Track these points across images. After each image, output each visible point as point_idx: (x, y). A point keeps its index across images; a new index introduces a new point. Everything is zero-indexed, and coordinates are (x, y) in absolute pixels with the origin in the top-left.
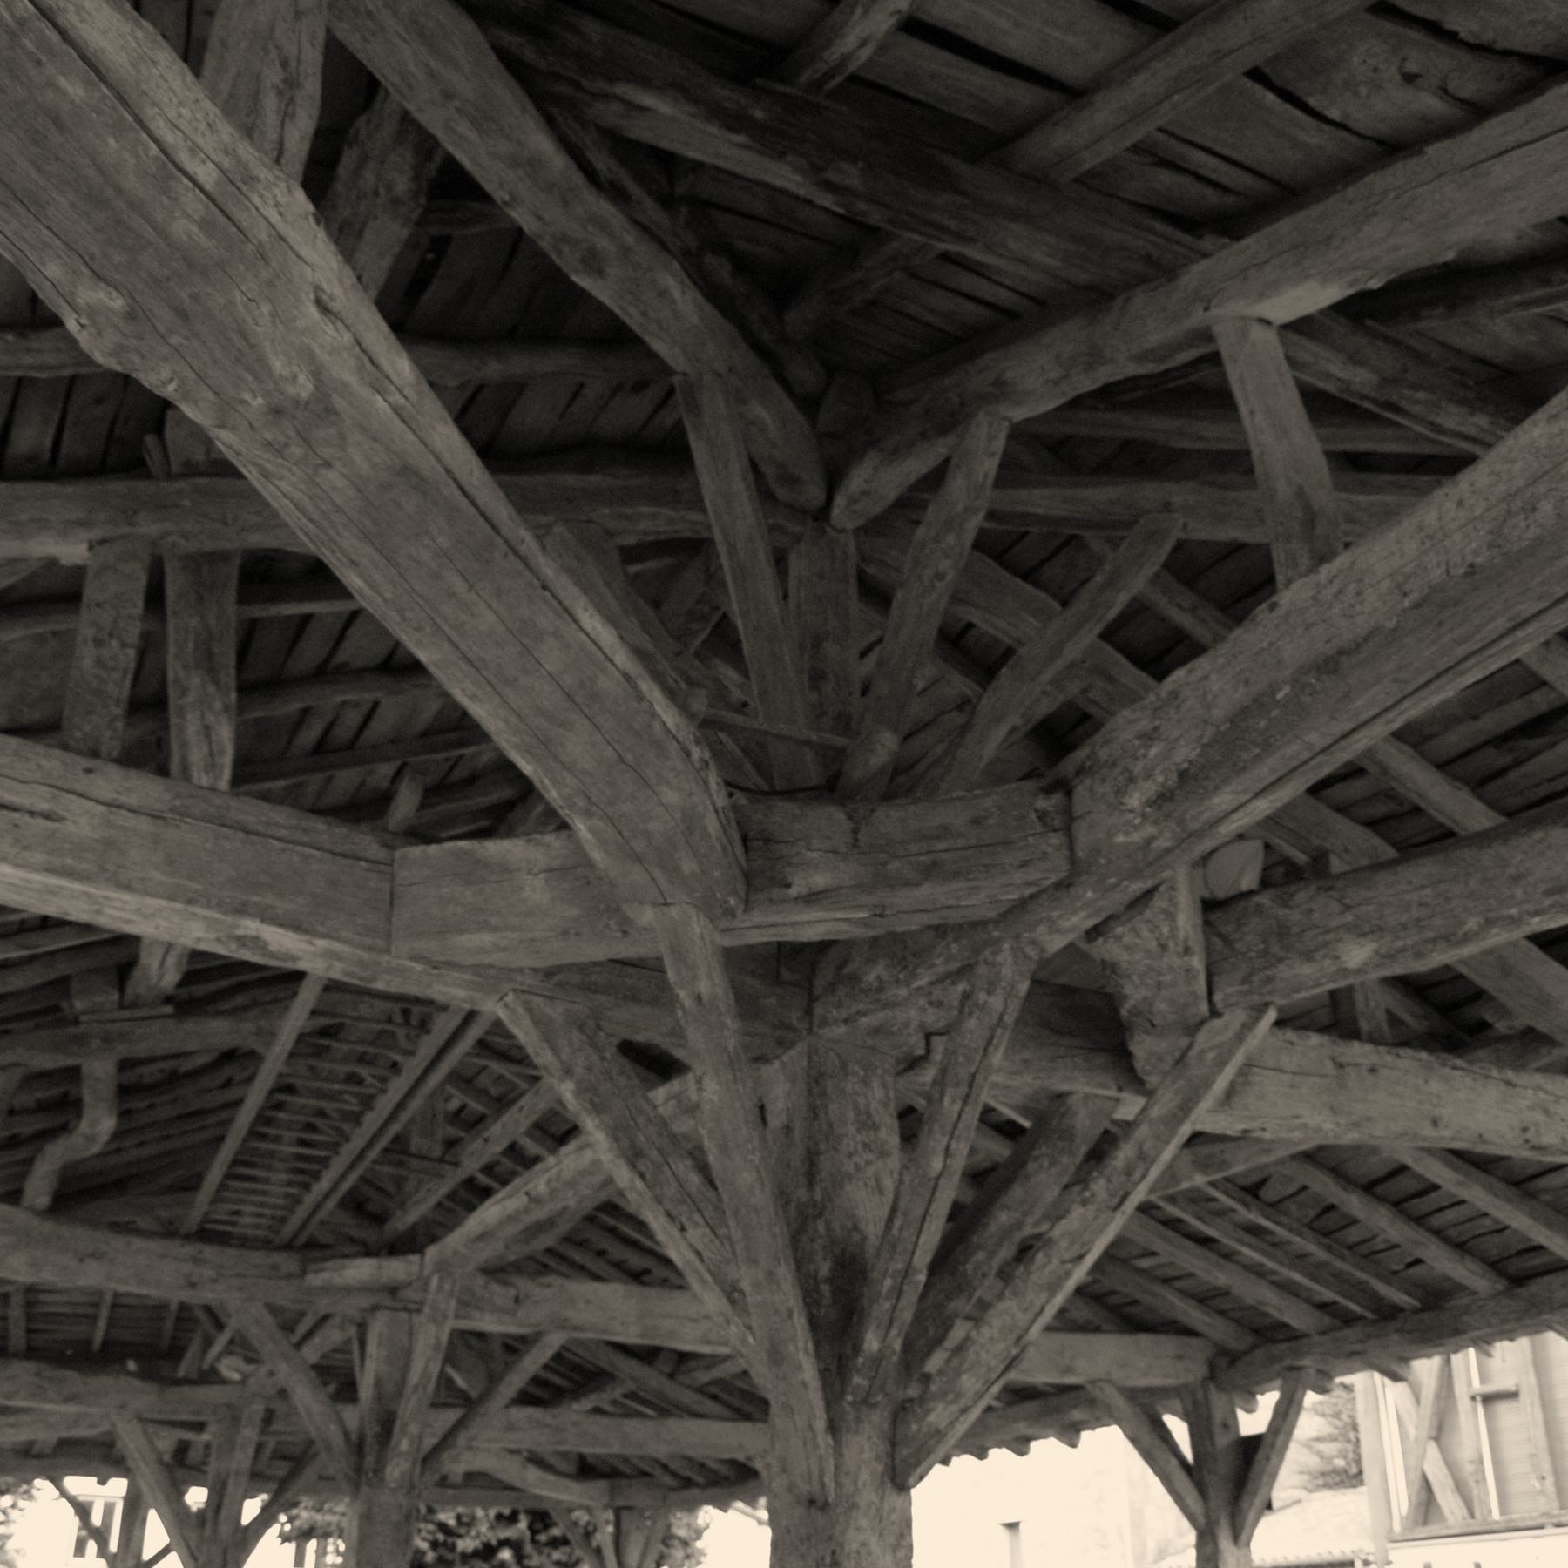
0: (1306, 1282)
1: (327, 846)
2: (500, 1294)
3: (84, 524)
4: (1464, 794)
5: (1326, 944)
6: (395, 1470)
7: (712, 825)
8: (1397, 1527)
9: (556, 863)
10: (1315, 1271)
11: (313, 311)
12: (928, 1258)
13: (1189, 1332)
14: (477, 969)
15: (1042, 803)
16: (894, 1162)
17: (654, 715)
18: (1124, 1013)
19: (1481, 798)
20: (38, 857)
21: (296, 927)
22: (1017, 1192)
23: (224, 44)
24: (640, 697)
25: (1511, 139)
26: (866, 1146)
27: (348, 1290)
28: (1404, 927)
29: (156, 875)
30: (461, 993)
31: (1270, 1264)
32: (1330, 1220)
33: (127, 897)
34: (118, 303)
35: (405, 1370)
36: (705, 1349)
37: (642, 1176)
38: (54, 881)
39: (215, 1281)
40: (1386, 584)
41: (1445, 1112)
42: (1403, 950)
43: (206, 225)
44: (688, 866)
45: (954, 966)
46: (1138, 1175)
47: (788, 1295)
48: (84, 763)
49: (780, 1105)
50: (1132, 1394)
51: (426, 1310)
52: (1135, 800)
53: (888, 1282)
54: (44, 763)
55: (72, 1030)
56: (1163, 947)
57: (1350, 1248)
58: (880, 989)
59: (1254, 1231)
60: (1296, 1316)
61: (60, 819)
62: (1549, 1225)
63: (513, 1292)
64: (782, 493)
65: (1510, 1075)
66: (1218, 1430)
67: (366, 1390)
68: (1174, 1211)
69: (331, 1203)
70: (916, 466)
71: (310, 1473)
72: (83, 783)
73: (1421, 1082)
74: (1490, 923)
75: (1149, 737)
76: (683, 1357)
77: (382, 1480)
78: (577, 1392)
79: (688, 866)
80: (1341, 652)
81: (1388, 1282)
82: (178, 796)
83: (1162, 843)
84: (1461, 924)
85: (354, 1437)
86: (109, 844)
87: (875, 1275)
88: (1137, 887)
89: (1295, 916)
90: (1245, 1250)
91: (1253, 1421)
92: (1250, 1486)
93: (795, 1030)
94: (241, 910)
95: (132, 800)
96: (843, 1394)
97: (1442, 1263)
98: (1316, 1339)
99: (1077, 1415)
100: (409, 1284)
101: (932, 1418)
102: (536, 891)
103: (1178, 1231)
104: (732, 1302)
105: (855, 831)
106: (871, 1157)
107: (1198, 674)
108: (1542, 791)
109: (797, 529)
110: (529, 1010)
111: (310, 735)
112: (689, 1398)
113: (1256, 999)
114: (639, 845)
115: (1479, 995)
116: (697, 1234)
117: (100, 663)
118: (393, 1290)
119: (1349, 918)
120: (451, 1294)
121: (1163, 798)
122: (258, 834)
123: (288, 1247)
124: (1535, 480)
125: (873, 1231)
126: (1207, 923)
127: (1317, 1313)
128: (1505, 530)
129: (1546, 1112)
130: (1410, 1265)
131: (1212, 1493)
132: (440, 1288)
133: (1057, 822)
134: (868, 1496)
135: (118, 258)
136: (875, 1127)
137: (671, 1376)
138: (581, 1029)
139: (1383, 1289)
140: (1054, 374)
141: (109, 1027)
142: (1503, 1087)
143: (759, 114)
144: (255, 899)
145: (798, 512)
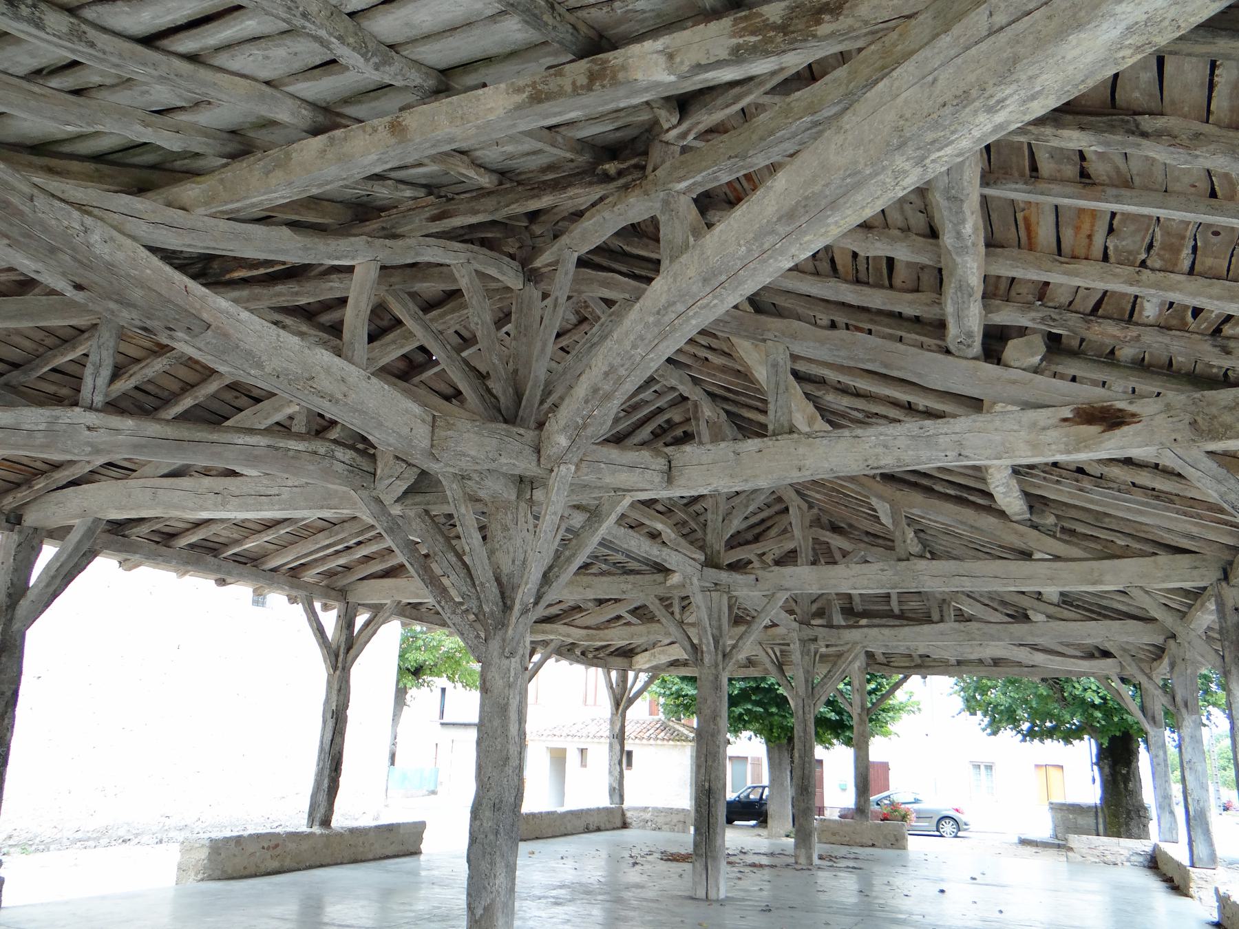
26: (505, 537)
63: (753, 577)
73: (792, 450)
95: (296, 484)
129: (886, 447)
134: (496, 660)
142: (851, 440)
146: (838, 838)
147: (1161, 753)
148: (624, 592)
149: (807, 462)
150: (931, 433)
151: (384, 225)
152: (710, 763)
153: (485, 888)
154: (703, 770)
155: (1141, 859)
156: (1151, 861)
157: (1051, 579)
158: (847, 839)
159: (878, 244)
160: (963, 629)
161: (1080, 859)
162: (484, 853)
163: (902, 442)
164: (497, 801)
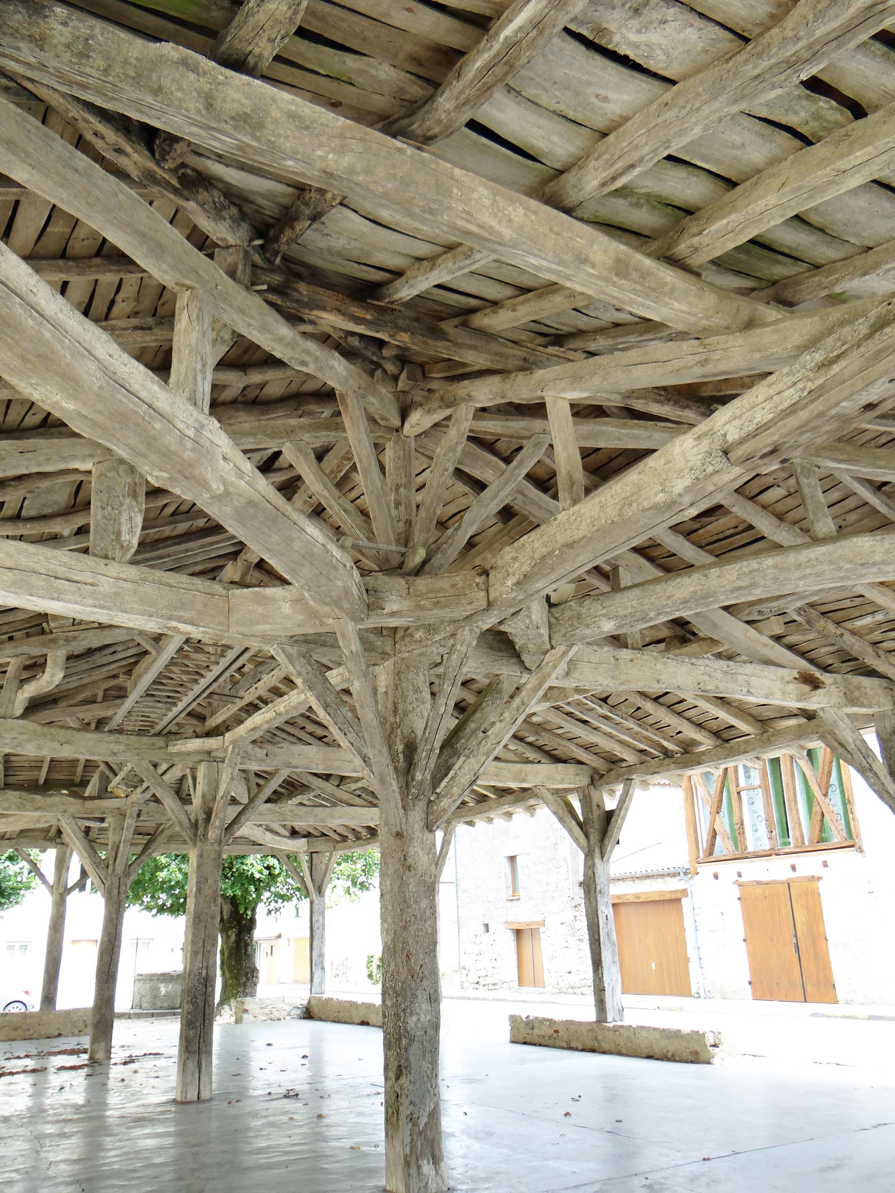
0: (631, 740)
1: (202, 590)
2: (260, 752)
3: (91, 456)
4: (681, 538)
5: (595, 622)
6: (213, 833)
7: (355, 590)
8: (701, 856)
9: (294, 598)
10: (636, 736)
11: (222, 462)
12: (440, 745)
13: (580, 763)
14: (263, 637)
15: (478, 580)
16: (428, 706)
17: (333, 556)
18: (517, 648)
19: (688, 540)
20: (90, 601)
21: (193, 624)
22: (478, 715)
23: (179, 349)
24: (328, 551)
25: (639, 360)
26: (417, 699)
27: (188, 754)
28: (626, 616)
29: (136, 606)
30: (256, 644)
31: (615, 733)
32: (640, 713)
33: (124, 615)
34: (166, 475)
35: (216, 789)
36: (355, 775)
37: (329, 714)
38: (96, 610)
39: (124, 752)
40: (589, 520)
41: (663, 677)
42: (626, 624)
43: (193, 450)
44: (346, 606)
45: (448, 634)
46: (521, 710)
47: (386, 759)
48: (104, 561)
49: (383, 683)
50: (556, 792)
51: (226, 761)
52: (509, 583)
53: (424, 753)
54: (88, 563)
55: (50, 637)
56: (528, 628)
57: (650, 726)
58: (421, 641)
59: (605, 717)
60: (631, 758)
61: (97, 585)
62: (736, 716)
63: (265, 752)
64: (382, 423)
65: (694, 660)
66: (594, 808)
67: (197, 800)
68: (569, 709)
69: (183, 715)
70: (438, 416)
71: (161, 839)
72: (105, 570)
73: (653, 665)
74: (659, 614)
75: (515, 559)
76: (342, 778)
77: (207, 839)
78: (290, 796)
79: (346, 606)
80: (574, 542)
81: (669, 741)
82: (142, 573)
83: (520, 597)
84: (648, 615)
85: (193, 820)
86: (117, 594)
87: (419, 751)
88: (513, 610)
89: (584, 610)
90: (602, 726)
91: (610, 804)
92: (609, 833)
93: (388, 654)
94: (170, 618)
95: (124, 576)
96: (408, 796)
97: (691, 733)
98: (638, 766)
99: (532, 802)
100: (217, 750)
101: (442, 804)
102: (287, 609)
103: (573, 718)
104: (365, 762)
105: (409, 589)
106: (419, 704)
107: (530, 539)
108: (715, 538)
109: (389, 436)
110: (284, 651)
111: (169, 510)
112: (346, 797)
113: (569, 643)
114: (327, 600)
115: (689, 623)
116: (351, 736)
117: (104, 517)
118: (209, 753)
119: (604, 611)
120: (238, 754)
121: (518, 583)
122: (175, 587)
123: (159, 734)
124: (632, 495)
125: (419, 733)
126: (550, 612)
127: (639, 754)
128: (47, 1143)
129: (710, 676)
130: (678, 733)
131: (592, 837)
132: (233, 752)
133: (483, 587)
134: (417, 834)
135: (169, 467)
136: (421, 692)
137: (338, 786)
138: (304, 658)
139: (666, 744)
140: (491, 397)
141: (68, 634)
142: (690, 666)
143: (369, 317)
144: (175, 613)
145: (390, 429)
146: (20, 1032)
147: (321, 918)
148: (115, 754)
149: (663, 677)
150: (733, 671)
151: (528, 357)
152: (208, 948)
153: (429, 1091)
154: (200, 956)
155: (299, 1012)
156: (306, 1013)
157: (497, 776)
158: (31, 1032)
159: (784, 534)
160: (278, 810)
161: (253, 1019)
162: (424, 1052)
163: (718, 674)
164: (432, 991)
